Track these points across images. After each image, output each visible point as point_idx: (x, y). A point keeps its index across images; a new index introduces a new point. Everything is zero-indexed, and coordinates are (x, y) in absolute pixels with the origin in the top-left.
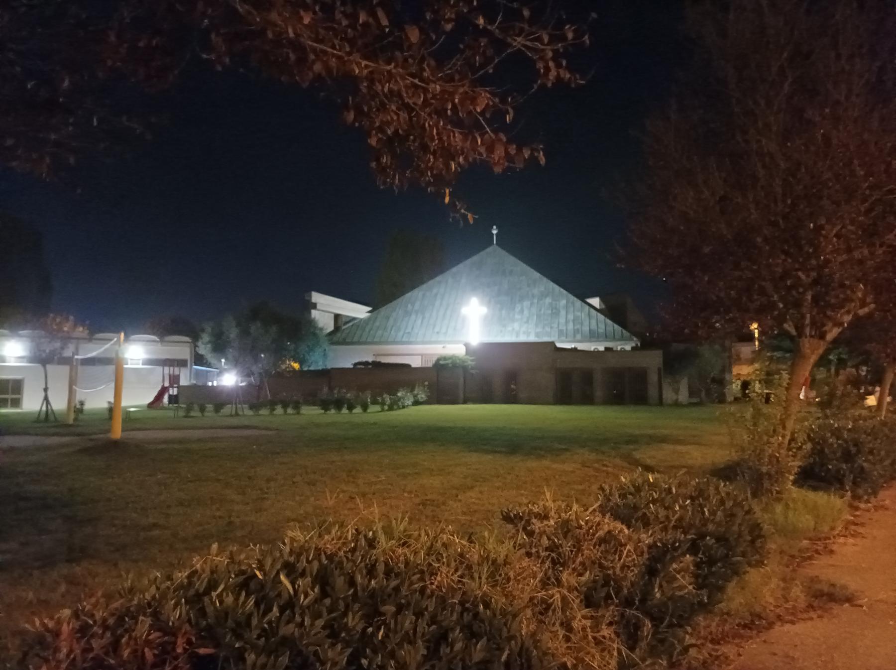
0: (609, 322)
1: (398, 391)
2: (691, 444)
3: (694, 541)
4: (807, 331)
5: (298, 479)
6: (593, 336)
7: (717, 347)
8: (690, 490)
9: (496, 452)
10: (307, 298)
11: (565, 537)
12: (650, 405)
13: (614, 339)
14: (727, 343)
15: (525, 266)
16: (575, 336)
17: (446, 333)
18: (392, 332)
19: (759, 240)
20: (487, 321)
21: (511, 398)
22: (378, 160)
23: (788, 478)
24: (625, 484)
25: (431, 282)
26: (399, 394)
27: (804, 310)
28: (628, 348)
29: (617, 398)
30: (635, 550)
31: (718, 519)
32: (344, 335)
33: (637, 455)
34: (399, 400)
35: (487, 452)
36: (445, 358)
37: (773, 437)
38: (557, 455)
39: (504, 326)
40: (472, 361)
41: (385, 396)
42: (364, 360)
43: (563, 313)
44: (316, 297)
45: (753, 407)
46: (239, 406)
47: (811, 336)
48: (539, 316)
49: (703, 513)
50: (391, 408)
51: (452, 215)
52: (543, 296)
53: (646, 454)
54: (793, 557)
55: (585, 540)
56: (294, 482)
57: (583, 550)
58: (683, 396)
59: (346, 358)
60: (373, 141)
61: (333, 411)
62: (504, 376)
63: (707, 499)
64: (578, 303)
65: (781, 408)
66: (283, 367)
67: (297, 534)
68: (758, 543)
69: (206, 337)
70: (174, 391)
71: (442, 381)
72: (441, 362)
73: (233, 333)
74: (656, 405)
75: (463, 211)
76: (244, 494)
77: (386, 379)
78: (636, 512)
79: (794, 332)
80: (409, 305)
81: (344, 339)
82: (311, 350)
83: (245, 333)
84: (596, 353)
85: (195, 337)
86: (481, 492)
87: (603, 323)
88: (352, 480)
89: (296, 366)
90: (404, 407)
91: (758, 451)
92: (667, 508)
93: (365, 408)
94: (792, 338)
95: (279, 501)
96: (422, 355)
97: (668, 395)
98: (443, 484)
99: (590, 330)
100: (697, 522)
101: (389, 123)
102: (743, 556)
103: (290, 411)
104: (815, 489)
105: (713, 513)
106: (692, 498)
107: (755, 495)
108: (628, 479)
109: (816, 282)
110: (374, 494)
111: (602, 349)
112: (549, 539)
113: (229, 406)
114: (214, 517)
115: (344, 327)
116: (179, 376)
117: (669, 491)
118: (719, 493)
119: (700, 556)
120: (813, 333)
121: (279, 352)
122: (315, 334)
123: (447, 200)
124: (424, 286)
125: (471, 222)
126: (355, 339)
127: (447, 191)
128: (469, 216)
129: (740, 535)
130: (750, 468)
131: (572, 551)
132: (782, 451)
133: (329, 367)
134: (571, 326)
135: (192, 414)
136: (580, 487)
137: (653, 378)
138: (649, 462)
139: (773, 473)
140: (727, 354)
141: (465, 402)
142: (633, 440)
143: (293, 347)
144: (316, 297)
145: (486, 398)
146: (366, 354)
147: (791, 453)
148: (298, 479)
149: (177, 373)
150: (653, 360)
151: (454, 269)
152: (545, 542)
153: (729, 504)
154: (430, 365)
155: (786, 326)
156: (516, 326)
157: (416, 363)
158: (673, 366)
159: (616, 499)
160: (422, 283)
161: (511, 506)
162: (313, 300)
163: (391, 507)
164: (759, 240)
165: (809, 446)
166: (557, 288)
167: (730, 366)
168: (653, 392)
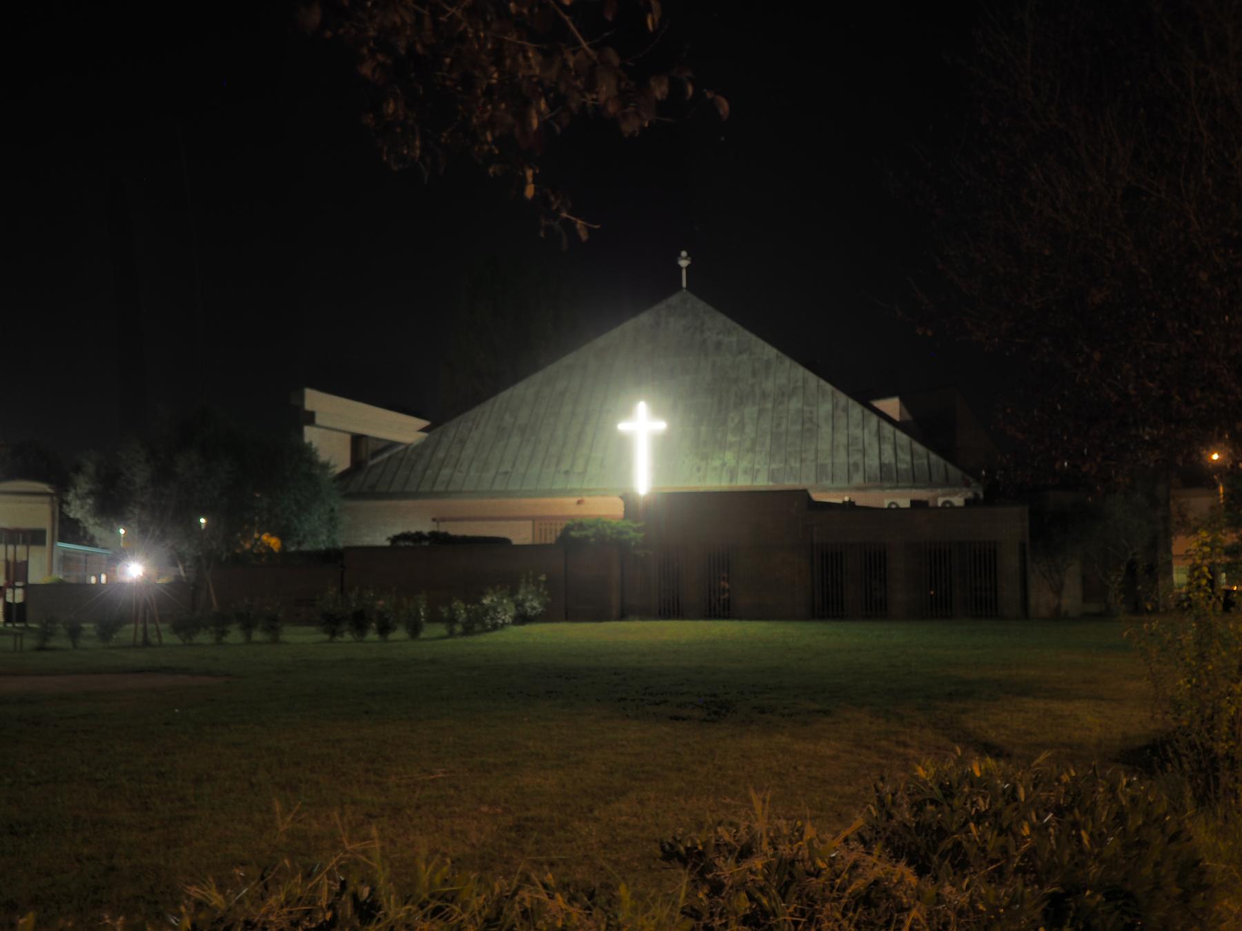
0: (918, 447)
1: (483, 594)
3: (1055, 899)
6: (887, 476)
9: (677, 718)
13: (930, 483)
16: (849, 479)
17: (584, 473)
24: (925, 783)
25: (552, 369)
26: (486, 601)
28: (958, 501)
29: (936, 607)
30: (929, 920)
34: (486, 613)
36: (581, 526)
39: (705, 457)
40: (637, 530)
42: (413, 530)
43: (826, 430)
44: (314, 400)
45: (1197, 618)
49: (1080, 839)
50: (468, 631)
55: (825, 900)
56: (252, 785)
57: (818, 922)
58: (1071, 599)
59: (378, 527)
61: (348, 637)
64: (856, 410)
70: (18, 596)
71: (582, 570)
72: (573, 533)
75: (564, 215)
77: (460, 568)
84: (894, 511)
86: (641, 802)
87: (900, 449)
89: (274, 542)
90: (495, 627)
91: (1209, 711)
93: (414, 629)
96: (533, 519)
97: (1041, 598)
98: (564, 786)
99: (881, 465)
103: (258, 636)
105: (1098, 839)
106: (1059, 811)
107: (1202, 800)
108: (932, 771)
110: (418, 807)
112: (751, 898)
115: (371, 463)
116: (26, 563)
117: (1012, 796)
118: (1115, 798)
123: (530, 191)
124: (538, 377)
125: (584, 236)
127: (529, 173)
128: (580, 224)
131: (796, 924)
133: (341, 545)
134: (841, 457)
135: (53, 643)
136: (849, 790)
141: (622, 617)
144: (314, 400)
145: (672, 610)
146: (414, 519)
149: (21, 557)
151: (601, 342)
152: (743, 905)
154: (551, 539)
156: (729, 457)
157: (521, 535)
159: (905, 814)
160: (536, 368)
161: (680, 830)
163: (453, 833)
164: (1204, 276)
166: (813, 380)
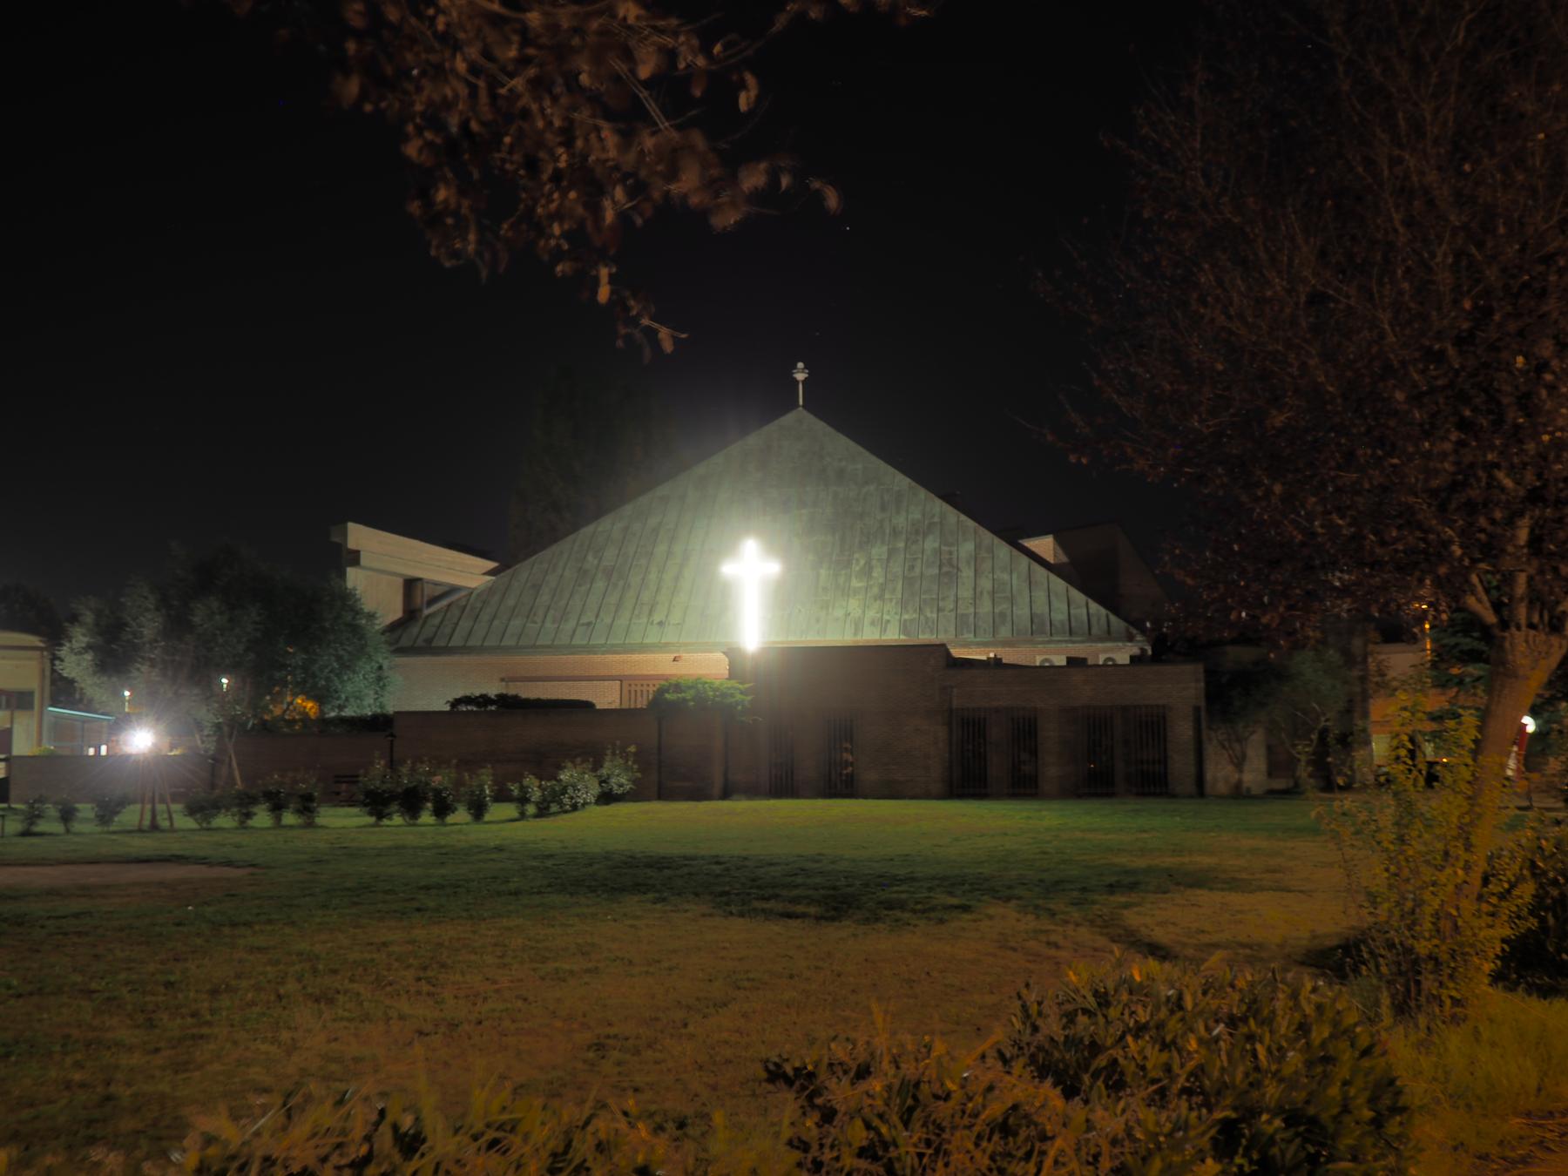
0: (1078, 596)
1: (560, 768)
2: (1262, 889)
3: (1228, 1127)
4: (1522, 612)
5: (291, 986)
6: (1039, 628)
7: (1332, 654)
8: (1232, 1003)
10: (336, 539)
11: (906, 1124)
12: (1174, 796)
13: (1090, 636)
14: (1357, 643)
15: (874, 458)
18: (548, 624)
19: (1399, 396)
20: (783, 597)
21: (840, 785)
22: (425, 194)
23: (1478, 969)
26: (564, 776)
27: (1507, 563)
28: (1123, 658)
29: (1095, 782)
31: (1287, 1071)
32: (428, 631)
33: (1132, 918)
34: (564, 791)
35: (768, 914)
36: (677, 687)
37: (1441, 869)
38: (941, 921)
41: (526, 782)
43: (967, 573)
46: (160, 807)
47: (1531, 626)
48: (908, 581)
50: (543, 812)
51: (623, 331)
52: (919, 531)
53: (1153, 916)
54: (1484, 1157)
56: (280, 997)
57: (946, 1153)
58: (1254, 774)
59: (421, 688)
60: (412, 150)
61: (397, 820)
62: (842, 728)
63: (1269, 1022)
64: (1003, 550)
65: (1460, 799)
66: (277, 711)
67: (219, 1123)
68: (1393, 1127)
69: (80, 637)
71: (671, 745)
73: (149, 625)
74: (1191, 797)
76: (151, 1024)
77: (534, 737)
78: (1094, 1055)
79: (1490, 618)
80: (590, 558)
81: (429, 641)
82: (346, 666)
83: (177, 625)
84: (1045, 673)
85: (52, 631)
87: (1065, 601)
88: (425, 988)
89: (310, 706)
90: (575, 808)
92: (1165, 1046)
93: (478, 810)
94: (1486, 633)
95: (235, 1043)
97: (1219, 772)
100: (1239, 1076)
101: (448, 105)
102: (1354, 1159)
103: (289, 818)
104: (1546, 993)
106: (1232, 1022)
107: (1401, 1009)
108: (1085, 976)
109: (1535, 497)
111: (1060, 660)
112: (868, 1126)
113: (138, 807)
114: (68, 1085)
115: (426, 612)
117: (1178, 1004)
118: (1297, 1006)
119: (1238, 1160)
120: (1536, 619)
121: (263, 672)
122: (355, 630)
123: (604, 293)
124: (628, 509)
125: (668, 346)
126: (456, 641)
127: (604, 273)
128: (664, 334)
129: (1346, 1109)
130: (1391, 946)
132: (1464, 903)
133: (391, 708)
135: (42, 826)
137: (1182, 731)
138: (1160, 936)
139: (1445, 957)
140: (1356, 673)
141: (726, 795)
142: (1128, 883)
143: (300, 659)
145: (784, 787)
147: (1485, 907)
148: (291, 986)
150: (1181, 688)
152: (859, 1136)
153: (1320, 1033)
154: (642, 703)
155: (1471, 601)
156: (854, 605)
157: (606, 697)
158: (1227, 698)
159: (1053, 1027)
162: (352, 544)
164: (1399, 396)
165: (1527, 890)
166: (952, 516)
167: (1365, 697)
168: (1180, 766)
